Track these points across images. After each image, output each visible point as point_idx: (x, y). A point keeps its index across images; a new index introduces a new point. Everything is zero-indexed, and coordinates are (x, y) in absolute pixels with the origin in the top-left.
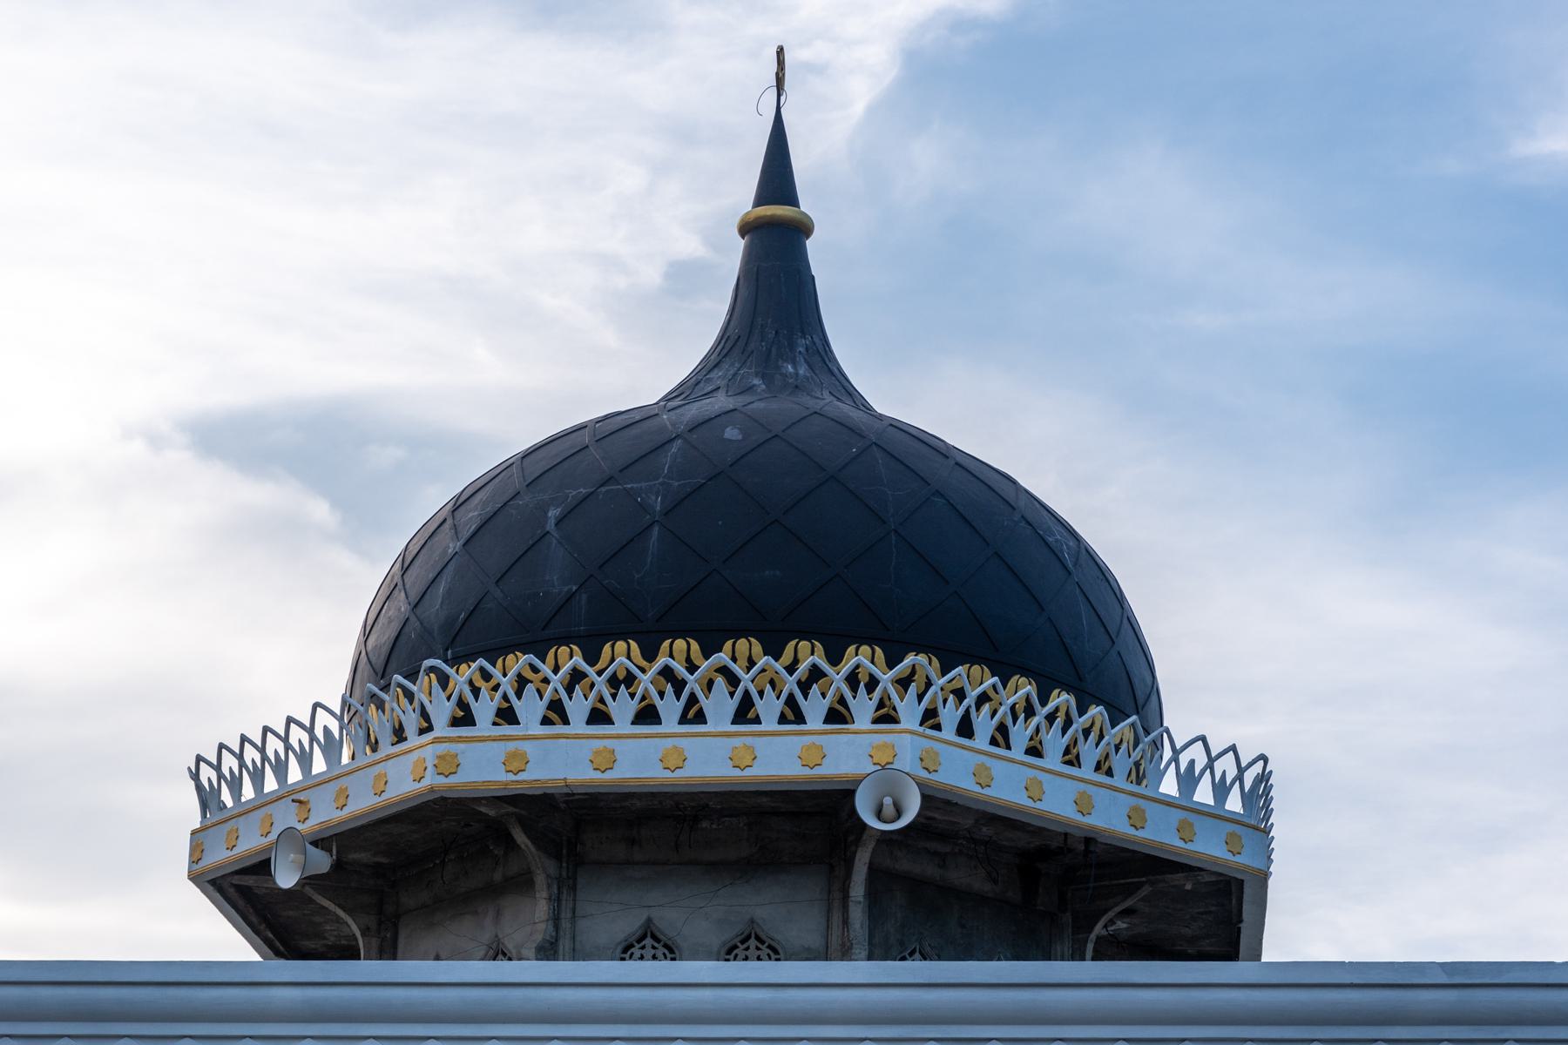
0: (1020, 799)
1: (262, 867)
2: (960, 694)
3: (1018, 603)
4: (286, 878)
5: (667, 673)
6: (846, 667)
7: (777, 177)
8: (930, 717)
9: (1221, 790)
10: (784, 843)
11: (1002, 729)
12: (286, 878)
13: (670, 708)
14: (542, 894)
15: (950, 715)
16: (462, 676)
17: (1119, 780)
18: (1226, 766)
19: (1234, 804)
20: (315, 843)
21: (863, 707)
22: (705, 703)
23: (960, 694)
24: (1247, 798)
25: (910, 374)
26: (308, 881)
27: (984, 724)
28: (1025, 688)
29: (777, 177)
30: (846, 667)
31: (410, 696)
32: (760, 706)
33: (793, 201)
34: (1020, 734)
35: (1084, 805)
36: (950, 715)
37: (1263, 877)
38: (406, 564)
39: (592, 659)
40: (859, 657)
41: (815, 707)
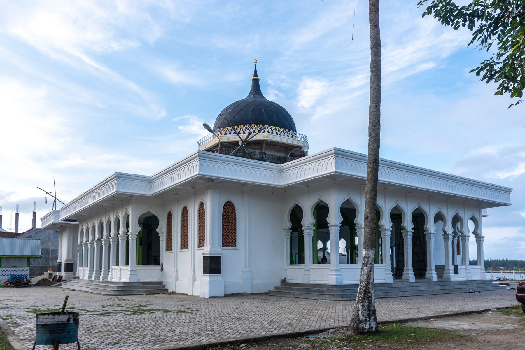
0: (279, 140)
2: (271, 129)
3: (281, 119)
5: (246, 128)
7: (256, 74)
8: (268, 132)
9: (301, 138)
15: (270, 131)
16: (225, 129)
18: (302, 136)
19: (303, 140)
20: (164, 50)
23: (271, 129)
24: (304, 139)
25: (270, 95)
27: (279, 133)
28: (283, 129)
29: (256, 74)
33: (257, 76)
34: (282, 134)
36: (270, 131)
38: (220, 116)
39: (263, 126)
40: (247, 126)
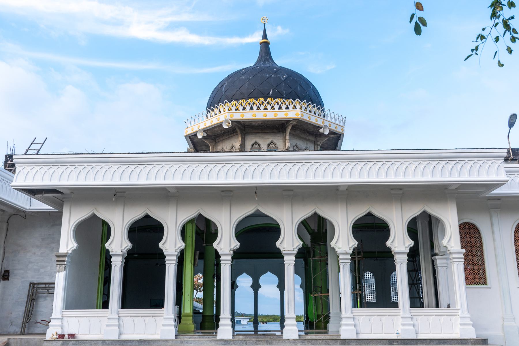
1: (196, 135)
2: (249, 104)
4: (200, 136)
6: (267, 101)
10: (277, 127)
11: (306, 108)
12: (200, 136)
13: (269, 107)
14: (240, 136)
17: (321, 117)
21: (269, 107)
22: (281, 106)
23: (249, 104)
26: (203, 137)
30: (267, 101)
31: (218, 108)
32: (275, 107)
35: (316, 120)
37: (343, 134)
39: (265, 101)
41: (262, 107)
